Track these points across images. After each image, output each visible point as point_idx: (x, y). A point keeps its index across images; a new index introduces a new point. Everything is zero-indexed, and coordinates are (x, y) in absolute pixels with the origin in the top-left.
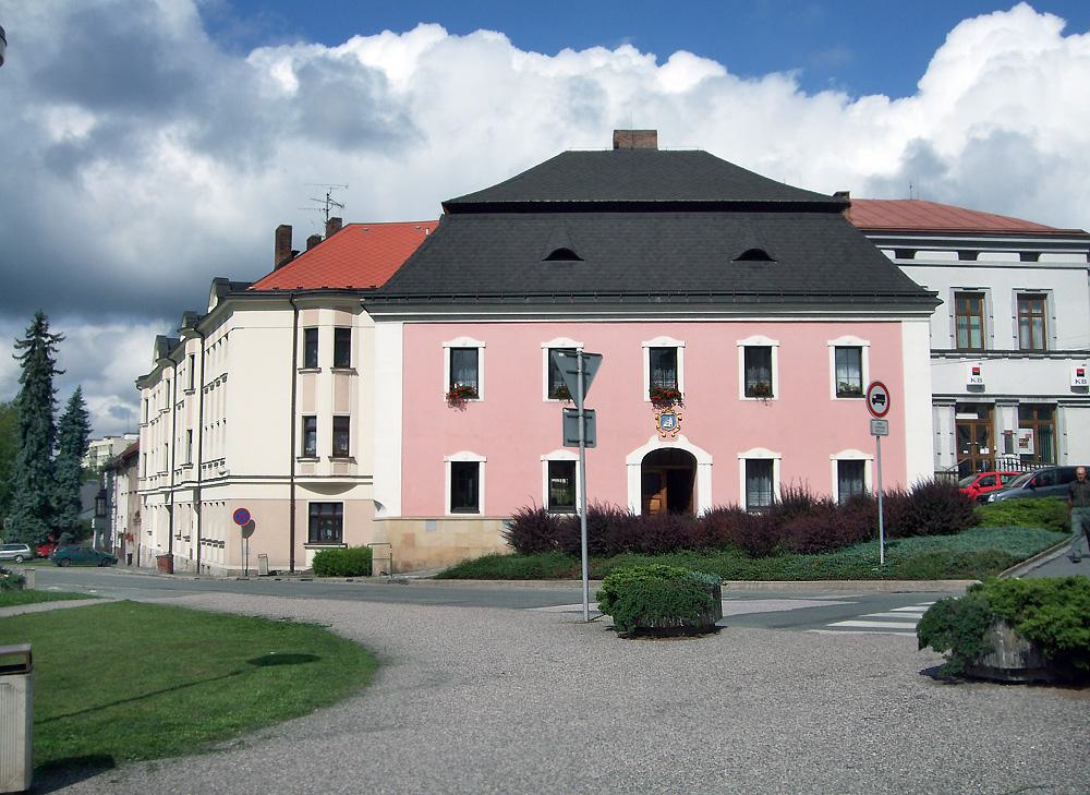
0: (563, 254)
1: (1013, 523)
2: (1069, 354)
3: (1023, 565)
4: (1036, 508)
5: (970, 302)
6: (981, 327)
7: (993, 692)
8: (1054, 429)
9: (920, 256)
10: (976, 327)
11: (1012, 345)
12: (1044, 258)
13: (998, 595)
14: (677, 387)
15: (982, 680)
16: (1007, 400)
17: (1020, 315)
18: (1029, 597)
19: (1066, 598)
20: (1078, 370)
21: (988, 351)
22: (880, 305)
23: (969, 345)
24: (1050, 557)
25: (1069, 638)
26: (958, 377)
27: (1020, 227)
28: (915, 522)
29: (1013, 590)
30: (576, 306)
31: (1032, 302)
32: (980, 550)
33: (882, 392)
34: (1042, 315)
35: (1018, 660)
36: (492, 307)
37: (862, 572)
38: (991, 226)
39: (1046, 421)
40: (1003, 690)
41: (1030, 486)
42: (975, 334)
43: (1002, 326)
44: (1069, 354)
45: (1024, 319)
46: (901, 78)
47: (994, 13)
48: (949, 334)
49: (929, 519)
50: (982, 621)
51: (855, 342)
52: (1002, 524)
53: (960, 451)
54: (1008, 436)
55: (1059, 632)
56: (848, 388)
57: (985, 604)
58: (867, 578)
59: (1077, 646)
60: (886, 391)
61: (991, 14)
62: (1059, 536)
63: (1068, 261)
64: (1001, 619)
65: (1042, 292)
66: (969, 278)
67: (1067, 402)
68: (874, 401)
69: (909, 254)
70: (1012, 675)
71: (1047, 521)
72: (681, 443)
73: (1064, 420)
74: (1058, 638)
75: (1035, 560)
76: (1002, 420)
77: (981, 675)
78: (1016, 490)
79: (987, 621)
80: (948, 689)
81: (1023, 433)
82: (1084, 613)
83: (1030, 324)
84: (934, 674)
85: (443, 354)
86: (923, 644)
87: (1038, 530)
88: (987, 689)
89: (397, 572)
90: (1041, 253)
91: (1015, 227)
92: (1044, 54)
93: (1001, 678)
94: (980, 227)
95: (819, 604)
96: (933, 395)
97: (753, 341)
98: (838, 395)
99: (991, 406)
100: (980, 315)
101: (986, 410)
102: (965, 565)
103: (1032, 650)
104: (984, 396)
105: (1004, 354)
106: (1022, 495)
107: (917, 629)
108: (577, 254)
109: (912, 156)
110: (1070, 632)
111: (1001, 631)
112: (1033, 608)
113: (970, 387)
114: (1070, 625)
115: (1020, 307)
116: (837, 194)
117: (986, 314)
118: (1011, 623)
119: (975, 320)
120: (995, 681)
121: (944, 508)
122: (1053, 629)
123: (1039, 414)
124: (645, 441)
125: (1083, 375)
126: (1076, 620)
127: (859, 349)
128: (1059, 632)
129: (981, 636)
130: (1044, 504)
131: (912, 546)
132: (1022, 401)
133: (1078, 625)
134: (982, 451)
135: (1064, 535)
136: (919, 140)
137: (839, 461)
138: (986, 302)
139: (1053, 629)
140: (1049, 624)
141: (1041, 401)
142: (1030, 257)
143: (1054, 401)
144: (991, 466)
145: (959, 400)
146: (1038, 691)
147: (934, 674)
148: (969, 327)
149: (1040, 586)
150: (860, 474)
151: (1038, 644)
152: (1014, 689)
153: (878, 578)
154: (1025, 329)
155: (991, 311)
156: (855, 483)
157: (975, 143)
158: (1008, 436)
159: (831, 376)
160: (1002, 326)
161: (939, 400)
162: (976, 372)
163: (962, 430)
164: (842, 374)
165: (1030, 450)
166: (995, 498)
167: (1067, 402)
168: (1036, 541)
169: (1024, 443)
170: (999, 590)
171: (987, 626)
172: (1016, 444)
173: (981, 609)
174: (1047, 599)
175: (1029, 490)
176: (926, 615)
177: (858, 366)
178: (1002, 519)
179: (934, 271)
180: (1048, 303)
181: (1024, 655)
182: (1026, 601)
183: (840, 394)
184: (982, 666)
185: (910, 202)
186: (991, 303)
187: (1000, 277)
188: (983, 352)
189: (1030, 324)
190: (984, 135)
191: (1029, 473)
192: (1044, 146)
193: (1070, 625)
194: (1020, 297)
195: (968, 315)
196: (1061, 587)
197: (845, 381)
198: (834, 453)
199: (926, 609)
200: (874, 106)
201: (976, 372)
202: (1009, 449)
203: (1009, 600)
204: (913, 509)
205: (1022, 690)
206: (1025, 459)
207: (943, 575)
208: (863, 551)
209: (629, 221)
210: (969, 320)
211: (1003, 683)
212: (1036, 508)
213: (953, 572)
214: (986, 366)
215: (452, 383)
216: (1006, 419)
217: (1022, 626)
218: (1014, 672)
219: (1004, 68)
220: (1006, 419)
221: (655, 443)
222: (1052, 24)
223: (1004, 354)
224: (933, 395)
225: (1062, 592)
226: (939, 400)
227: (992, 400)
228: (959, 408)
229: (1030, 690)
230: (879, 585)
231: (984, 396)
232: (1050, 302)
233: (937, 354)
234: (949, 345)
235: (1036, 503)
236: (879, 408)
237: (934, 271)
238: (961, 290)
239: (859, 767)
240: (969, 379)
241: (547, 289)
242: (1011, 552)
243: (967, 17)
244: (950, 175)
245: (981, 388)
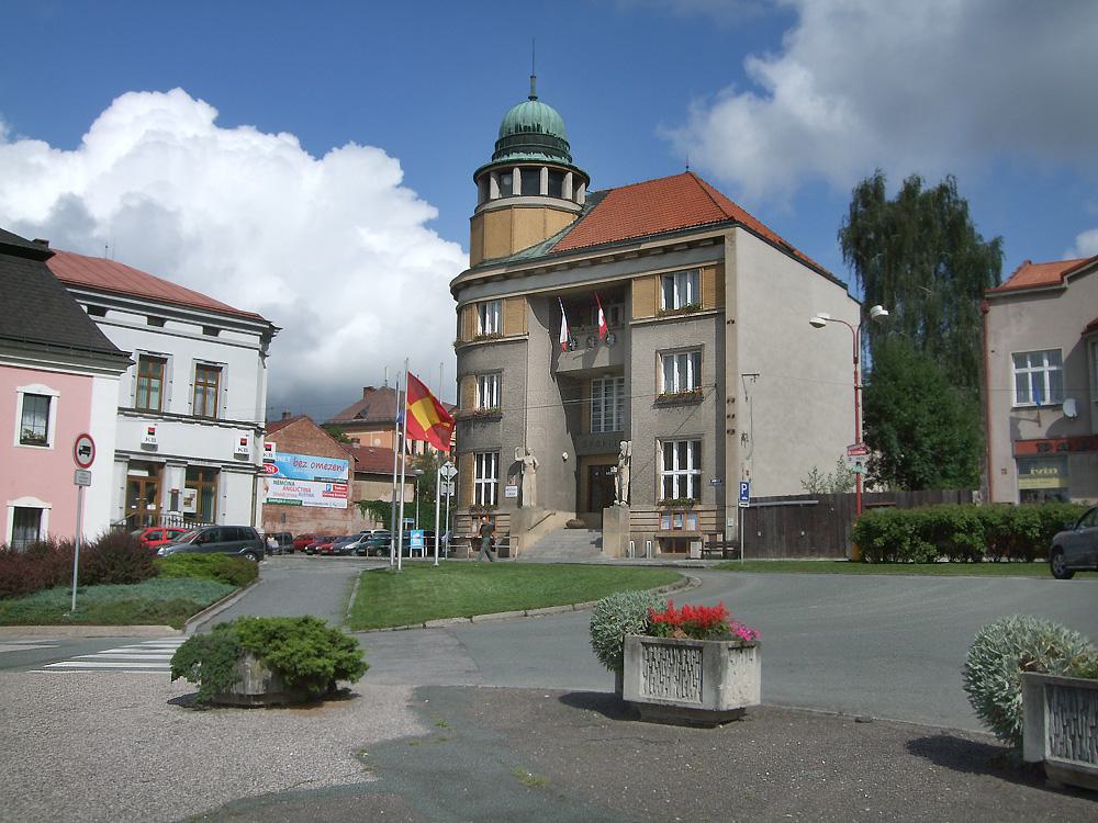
1: (188, 575)
2: (236, 424)
3: (205, 613)
4: (207, 562)
5: (153, 365)
6: (160, 390)
7: (240, 714)
8: (216, 490)
9: (111, 315)
10: (155, 389)
11: (186, 410)
13: (249, 632)
15: (227, 706)
16: (176, 461)
17: (197, 383)
18: (275, 633)
19: (304, 633)
20: (150, 429)
21: (164, 414)
22: (77, 358)
23: (144, 408)
24: (224, 607)
25: (307, 666)
26: (136, 434)
27: (205, 303)
28: (99, 570)
29: (262, 627)
30: (28, 352)
31: (208, 372)
32: (168, 599)
33: (89, 444)
34: (216, 386)
35: (261, 687)
37: (53, 618)
38: (180, 297)
39: (208, 484)
40: (248, 712)
41: (197, 542)
42: (154, 396)
43: (179, 391)
44: (236, 424)
45: (199, 387)
46: (67, 134)
47: (155, 93)
48: (130, 393)
49: (113, 568)
50: (233, 654)
51: (45, 391)
52: (178, 576)
53: (128, 505)
54: (175, 494)
55: (300, 661)
56: (32, 436)
57: (236, 641)
58: (59, 623)
59: (313, 673)
60: (92, 442)
61: (152, 92)
62: (228, 588)
63: (188, 330)
64: (249, 651)
66: (154, 343)
67: (229, 467)
68: (81, 452)
69: (102, 312)
70: (254, 700)
71: (217, 574)
73: (225, 483)
74: (299, 666)
75: (213, 609)
76: (171, 479)
77: (226, 701)
78: (184, 545)
79: (238, 655)
80: (200, 715)
81: (188, 493)
82: (318, 646)
83: (205, 393)
84: (185, 702)
85: (16, 397)
86: (176, 674)
87: (211, 582)
88: (233, 713)
90: (109, 309)
91: (201, 302)
92: (196, 138)
93: (245, 703)
94: (148, 293)
95: (16, 648)
96: (116, 451)
98: (22, 442)
99: (162, 465)
100: (161, 379)
101: (156, 469)
102: (156, 612)
103: (273, 677)
104: (157, 455)
105: (179, 418)
106: (188, 550)
107: (172, 662)
109: (61, 208)
110: (308, 662)
111: (250, 663)
112: (278, 642)
113: (144, 446)
114: (308, 655)
115: (198, 376)
116: (36, 241)
117: (166, 379)
118: (257, 656)
119: (155, 383)
120: (239, 706)
121: (129, 558)
122: (295, 659)
123: (203, 476)
125: (153, 434)
126: (313, 651)
127: (49, 398)
128: (300, 661)
129: (230, 667)
130: (215, 558)
131: (102, 594)
132: (191, 463)
133: (315, 656)
134: (149, 507)
135: (233, 587)
136: (72, 195)
137: (15, 507)
138: (167, 367)
139: (295, 659)
140: (292, 655)
141: (207, 464)
142: (157, 322)
143: (219, 465)
144: (157, 520)
145: (133, 457)
146: (276, 712)
147: (185, 702)
148: (149, 389)
149: (283, 623)
150: (36, 521)
151: (280, 672)
152: (257, 712)
153: (70, 623)
154: (199, 396)
155: (171, 377)
156: (29, 531)
157: (127, 210)
158: (175, 494)
159: (18, 423)
160: (179, 391)
161: (120, 455)
162: (152, 432)
163: (133, 486)
164: (28, 421)
165: (192, 509)
166: (164, 552)
167: (229, 467)
168: (211, 592)
169: (188, 502)
170: (248, 627)
171: (237, 658)
172: (181, 502)
173: (233, 644)
174: (290, 634)
175: (196, 546)
176: (179, 650)
177: (45, 415)
178: (178, 571)
179: (124, 330)
180: (222, 375)
181: (266, 683)
182: (272, 636)
183: (24, 441)
184: (229, 694)
185: (105, 261)
186: (172, 369)
187: (183, 347)
188: (215, 421)
189: (205, 393)
190: (134, 203)
191: (194, 531)
192: (188, 226)
193: (308, 655)
195: (150, 377)
196: (299, 625)
197: (30, 429)
198: (12, 499)
199: (179, 646)
200: (36, 151)
201: (152, 432)
202: (174, 507)
203: (258, 635)
204: (99, 557)
205: (263, 712)
206: (188, 517)
207: (135, 621)
208: (55, 596)
210: (149, 383)
211: (246, 707)
212: (207, 562)
213: (144, 618)
214: (162, 427)
216: (174, 478)
217: (268, 658)
218: (257, 697)
219: (158, 143)
220: (174, 478)
222: (204, 113)
223: (179, 418)
224: (116, 451)
225: (301, 629)
226: (120, 455)
227: (163, 460)
228: (133, 464)
229: (270, 712)
230: (71, 631)
231: (157, 455)
232: (169, 367)
233: (121, 410)
234: (130, 404)
235: (208, 558)
236: (84, 459)
237: (124, 330)
239: (154, 780)
240: (144, 438)
242: (195, 601)
243: (133, 91)
244: (96, 233)
245: (154, 447)
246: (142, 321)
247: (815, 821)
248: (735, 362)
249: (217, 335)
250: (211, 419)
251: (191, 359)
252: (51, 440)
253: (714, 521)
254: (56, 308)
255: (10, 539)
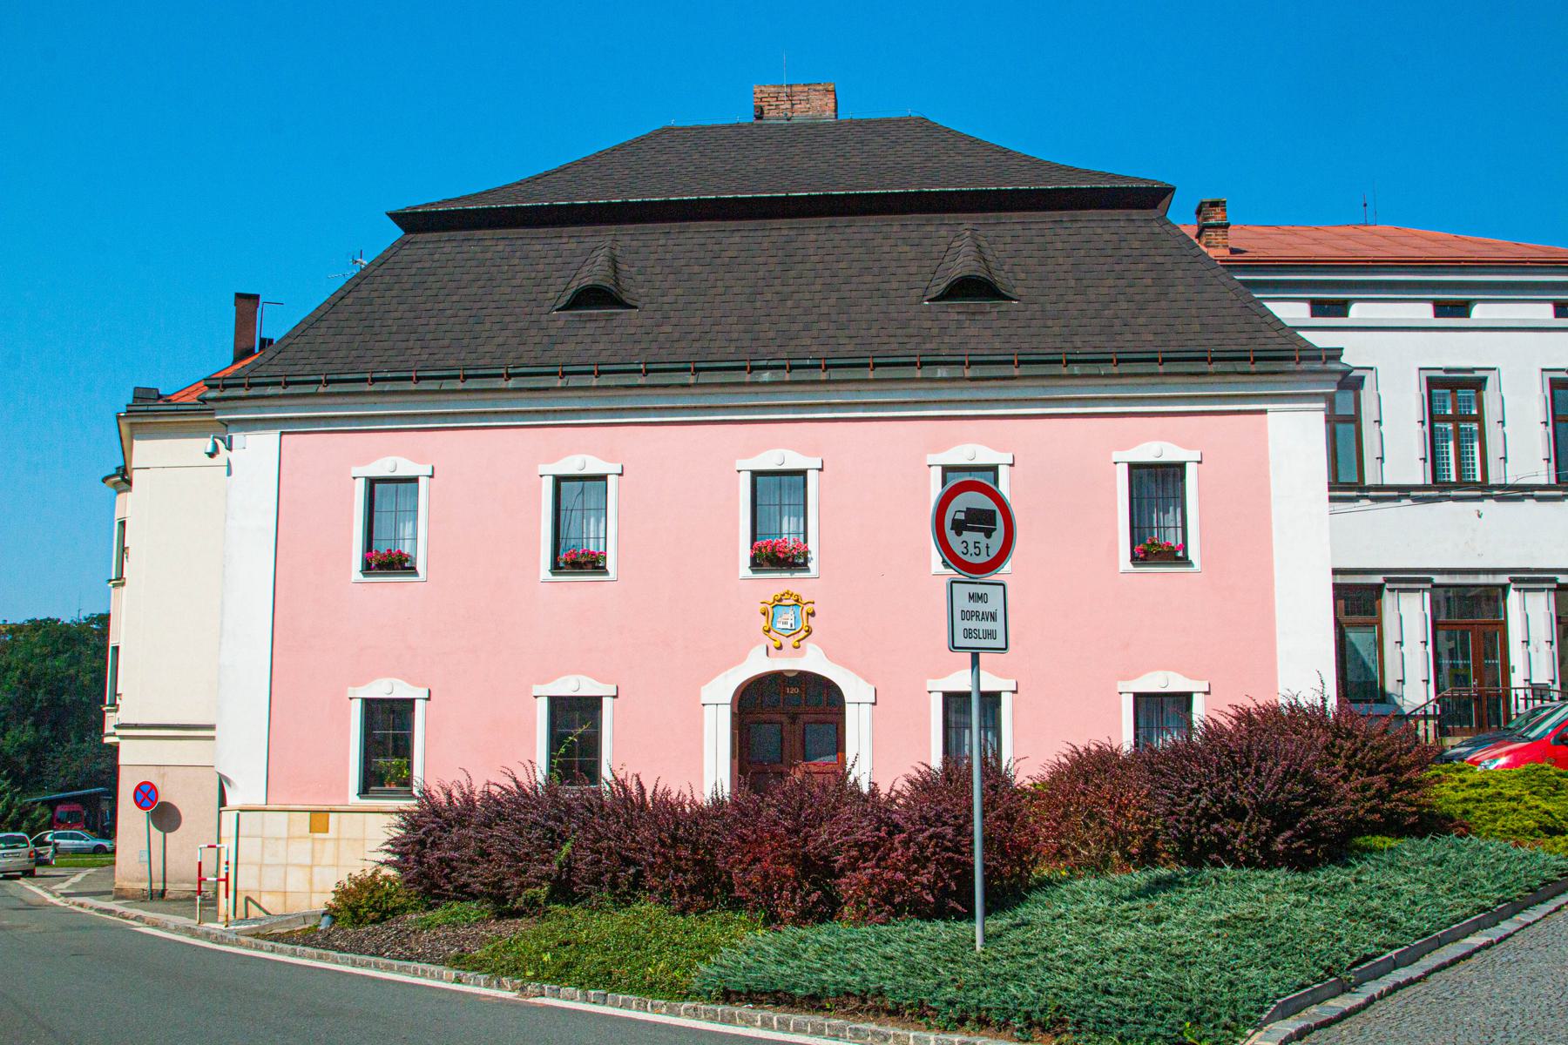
0: (592, 297)
12: (1480, 313)
14: (806, 540)
21: (1370, 488)
36: (1241, 386)
51: (1171, 454)
65: (1478, 374)
72: (812, 661)
85: (928, 474)
89: (1110, 993)
94: (1476, 256)
96: (1335, 572)
97: (1149, 452)
105: (1402, 492)
108: (624, 296)
124: (740, 659)
188: (1485, 490)
194: (1432, 383)
198: (356, 684)
209: (734, 237)
215: (754, 538)
221: (759, 663)
223: (1402, 492)
224: (1335, 572)
238: (1441, 374)
241: (553, 361)
246: (1423, 312)
247: (1566, 1015)
248: (1544, 320)
249: (1346, 316)
250: (1473, 485)
251: (1537, 373)
252: (1193, 553)
253: (591, 549)
254: (1181, 289)
255: (940, 755)
